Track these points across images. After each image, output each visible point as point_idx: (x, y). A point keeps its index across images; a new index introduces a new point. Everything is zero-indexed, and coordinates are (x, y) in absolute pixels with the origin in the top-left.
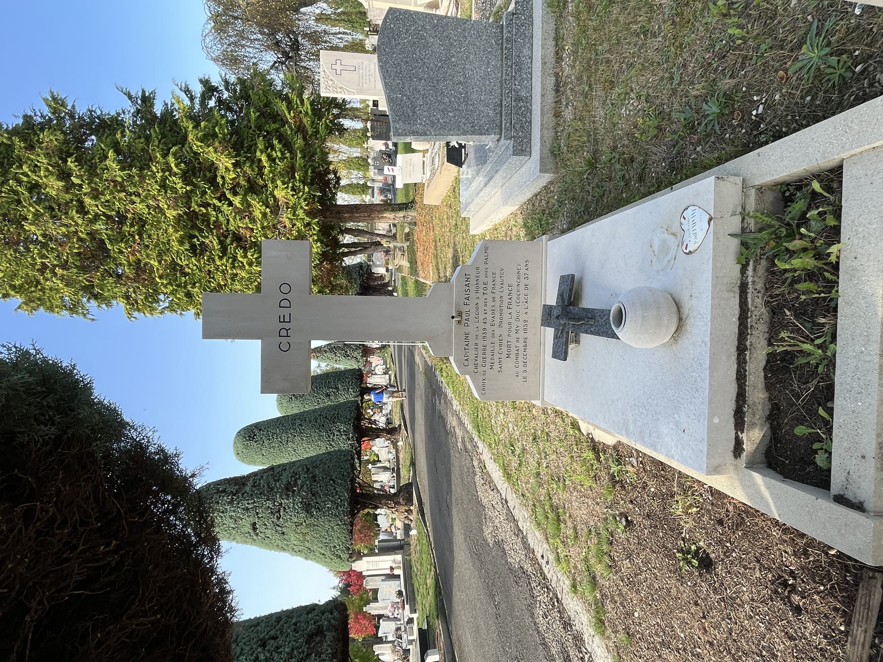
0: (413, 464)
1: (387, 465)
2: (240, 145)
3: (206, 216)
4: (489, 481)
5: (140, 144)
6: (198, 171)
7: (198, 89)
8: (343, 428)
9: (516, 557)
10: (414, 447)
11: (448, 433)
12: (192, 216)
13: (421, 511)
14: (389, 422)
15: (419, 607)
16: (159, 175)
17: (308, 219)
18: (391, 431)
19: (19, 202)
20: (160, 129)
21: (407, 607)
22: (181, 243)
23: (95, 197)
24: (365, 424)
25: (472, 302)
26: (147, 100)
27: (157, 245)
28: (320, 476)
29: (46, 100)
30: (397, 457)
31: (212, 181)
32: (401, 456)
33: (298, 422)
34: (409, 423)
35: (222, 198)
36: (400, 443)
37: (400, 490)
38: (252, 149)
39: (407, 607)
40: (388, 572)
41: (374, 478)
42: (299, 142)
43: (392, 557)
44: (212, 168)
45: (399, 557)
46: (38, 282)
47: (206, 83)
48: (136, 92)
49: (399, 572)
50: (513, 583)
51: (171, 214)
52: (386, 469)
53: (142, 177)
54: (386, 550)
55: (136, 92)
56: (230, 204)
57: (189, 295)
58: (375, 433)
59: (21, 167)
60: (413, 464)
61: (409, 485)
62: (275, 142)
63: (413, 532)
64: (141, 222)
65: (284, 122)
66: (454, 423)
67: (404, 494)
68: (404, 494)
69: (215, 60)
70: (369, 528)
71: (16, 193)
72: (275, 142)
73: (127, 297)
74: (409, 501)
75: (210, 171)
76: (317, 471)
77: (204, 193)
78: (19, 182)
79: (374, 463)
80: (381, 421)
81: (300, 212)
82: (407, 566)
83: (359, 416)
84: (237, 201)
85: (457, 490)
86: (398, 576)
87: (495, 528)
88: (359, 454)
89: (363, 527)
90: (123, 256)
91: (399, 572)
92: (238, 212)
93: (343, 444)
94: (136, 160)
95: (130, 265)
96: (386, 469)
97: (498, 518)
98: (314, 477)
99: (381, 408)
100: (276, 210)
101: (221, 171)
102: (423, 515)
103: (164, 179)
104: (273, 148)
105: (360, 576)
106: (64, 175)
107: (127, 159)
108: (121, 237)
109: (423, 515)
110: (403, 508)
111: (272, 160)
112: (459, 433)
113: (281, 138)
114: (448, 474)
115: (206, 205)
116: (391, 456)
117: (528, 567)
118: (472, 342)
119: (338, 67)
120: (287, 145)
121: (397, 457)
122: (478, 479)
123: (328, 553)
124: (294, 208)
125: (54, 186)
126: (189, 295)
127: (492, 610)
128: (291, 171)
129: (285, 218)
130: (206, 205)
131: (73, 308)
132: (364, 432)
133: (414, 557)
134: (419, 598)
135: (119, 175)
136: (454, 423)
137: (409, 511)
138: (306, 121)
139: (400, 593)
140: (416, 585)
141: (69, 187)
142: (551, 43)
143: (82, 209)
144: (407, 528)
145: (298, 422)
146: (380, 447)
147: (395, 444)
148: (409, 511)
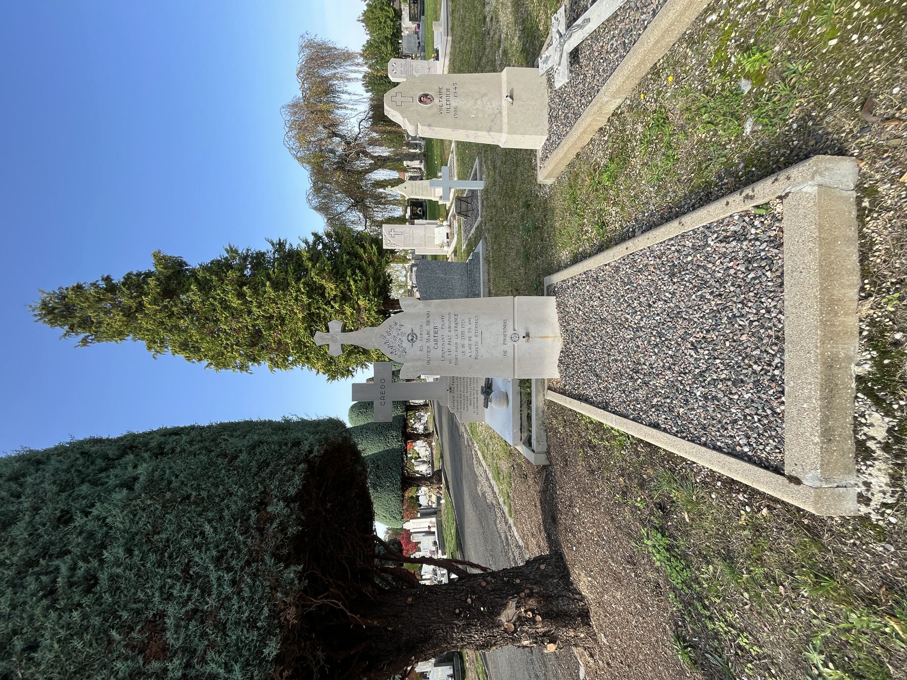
0: (442, 457)
1: (425, 459)
2: (337, 274)
3: (319, 314)
4: (479, 462)
5: (282, 275)
6: (316, 291)
7: (311, 239)
8: (395, 434)
9: (490, 498)
10: (442, 446)
11: (461, 436)
12: (311, 315)
13: (448, 488)
14: (426, 429)
15: (447, 550)
16: (294, 294)
17: (377, 316)
18: (427, 436)
19: (214, 310)
20: (289, 259)
21: (440, 551)
22: (305, 329)
23: (259, 307)
24: (409, 430)
25: (455, 384)
26: (281, 245)
27: (290, 331)
28: (381, 466)
29: (226, 250)
30: (432, 453)
31: (322, 295)
32: (434, 452)
33: (364, 431)
34: (438, 430)
35: (328, 303)
36: (433, 444)
37: (434, 473)
38: (343, 275)
39: (440, 551)
40: (427, 529)
41: (416, 469)
42: (370, 270)
43: (429, 520)
44: (322, 288)
45: (434, 520)
46: (223, 353)
47: (315, 235)
48: (275, 241)
49: (434, 529)
50: (486, 510)
51: (300, 316)
52: (424, 462)
53: (285, 295)
54: (425, 515)
55: (275, 241)
56: (332, 307)
57: (308, 358)
58: (417, 437)
59: (215, 290)
60: (442, 457)
61: (440, 471)
62: (357, 271)
63: (443, 501)
64: (282, 319)
65: (361, 259)
66: (463, 430)
67: (435, 478)
68: (435, 478)
69: (315, 208)
70: (413, 507)
71: (212, 304)
72: (357, 271)
73: (271, 360)
74: (440, 481)
75: (321, 290)
76: (379, 463)
77: (318, 302)
78: (215, 299)
79: (416, 459)
80: (420, 428)
81: (373, 313)
82: (439, 525)
83: (405, 425)
84: (336, 306)
85: (465, 469)
86: (434, 533)
87: (483, 487)
88: (406, 451)
89: (408, 506)
90: (271, 337)
91: (434, 529)
92: (337, 311)
93: (395, 445)
94: (280, 285)
95: (275, 342)
96: (424, 462)
97: (482, 480)
98: (378, 466)
99: (420, 419)
100: (359, 310)
101: (328, 290)
102: (448, 490)
103: (297, 296)
104: (356, 275)
105: (408, 533)
106: (241, 295)
107: (276, 286)
108: (270, 328)
109: (448, 490)
110: (436, 486)
111: (355, 281)
112: (465, 436)
113: (360, 268)
114: (461, 460)
115: (319, 308)
116: (427, 453)
117: (494, 502)
118: (456, 399)
119: (393, 233)
120: (364, 272)
121: (432, 453)
122: (475, 462)
123: (388, 516)
124: (369, 310)
125: (236, 303)
126: (308, 358)
127: (481, 531)
128: (367, 289)
129: (364, 315)
130: (319, 308)
131: (242, 367)
132: (410, 436)
133: (444, 518)
134: (447, 545)
135: (273, 294)
136: (463, 430)
137: (440, 488)
138: (375, 259)
139: (435, 543)
140: (445, 536)
141: (245, 302)
142: (486, 275)
143: (250, 312)
144: (439, 499)
145: (364, 431)
146: (420, 447)
147: (430, 444)
148: (440, 488)
